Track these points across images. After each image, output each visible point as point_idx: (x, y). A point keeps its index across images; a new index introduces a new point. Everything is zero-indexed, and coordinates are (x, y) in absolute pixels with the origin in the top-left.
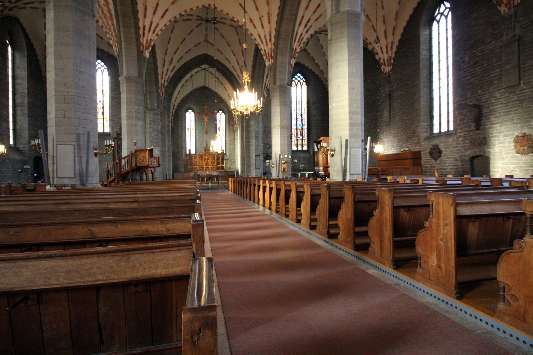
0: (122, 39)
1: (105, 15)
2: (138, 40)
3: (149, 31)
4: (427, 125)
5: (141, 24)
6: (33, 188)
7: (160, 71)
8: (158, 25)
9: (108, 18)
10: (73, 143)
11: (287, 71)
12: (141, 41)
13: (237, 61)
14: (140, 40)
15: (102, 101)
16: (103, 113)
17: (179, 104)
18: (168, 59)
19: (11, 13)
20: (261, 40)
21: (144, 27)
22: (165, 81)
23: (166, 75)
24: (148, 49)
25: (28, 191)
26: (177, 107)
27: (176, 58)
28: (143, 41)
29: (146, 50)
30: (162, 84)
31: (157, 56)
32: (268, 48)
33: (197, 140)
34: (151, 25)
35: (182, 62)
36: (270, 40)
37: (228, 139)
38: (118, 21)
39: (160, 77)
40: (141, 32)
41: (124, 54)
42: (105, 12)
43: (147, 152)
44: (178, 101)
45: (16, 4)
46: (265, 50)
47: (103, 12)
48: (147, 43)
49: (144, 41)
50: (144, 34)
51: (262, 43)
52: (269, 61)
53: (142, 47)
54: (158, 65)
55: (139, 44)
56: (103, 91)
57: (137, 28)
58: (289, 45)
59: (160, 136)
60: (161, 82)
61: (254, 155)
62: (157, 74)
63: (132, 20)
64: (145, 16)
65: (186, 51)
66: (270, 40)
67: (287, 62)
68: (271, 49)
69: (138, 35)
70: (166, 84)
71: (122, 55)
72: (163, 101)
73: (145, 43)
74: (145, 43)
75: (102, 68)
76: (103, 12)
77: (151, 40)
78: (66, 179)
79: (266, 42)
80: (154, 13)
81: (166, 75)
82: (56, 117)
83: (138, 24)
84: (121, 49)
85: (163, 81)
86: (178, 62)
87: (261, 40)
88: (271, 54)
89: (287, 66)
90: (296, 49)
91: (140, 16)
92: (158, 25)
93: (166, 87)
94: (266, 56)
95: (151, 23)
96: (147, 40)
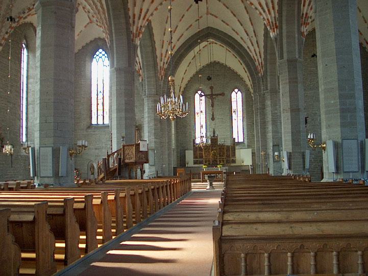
0: (113, 31)
1: (98, 10)
2: (128, 29)
3: (139, 19)
5: (131, 13)
6: (26, 185)
7: (158, 53)
8: (148, 10)
9: (101, 13)
10: (51, 145)
11: (297, 41)
12: (131, 30)
13: (246, 32)
14: (130, 29)
15: (102, 92)
16: (103, 104)
17: (186, 85)
18: (167, 38)
19: (26, 20)
20: (263, 8)
21: (134, 15)
22: (164, 63)
23: (165, 57)
24: (139, 36)
25: (22, 188)
26: (185, 89)
27: (175, 36)
28: (133, 29)
29: (136, 37)
30: (161, 67)
31: (155, 37)
32: (271, 17)
33: (208, 125)
34: (141, 12)
35: (182, 40)
36: (273, 8)
37: (245, 123)
38: (109, 15)
39: (158, 60)
40: (131, 21)
41: (115, 46)
42: (99, 8)
43: (134, 148)
44: (185, 82)
45: (29, 13)
46: (268, 19)
47: (97, 8)
48: (137, 31)
49: (134, 29)
50: (134, 22)
51: (264, 11)
52: (274, 31)
53: (132, 35)
54: (156, 47)
55: (129, 32)
56: (103, 80)
57: (127, 17)
58: (296, 11)
59: (159, 125)
60: (160, 64)
61: (271, 144)
62: (155, 57)
63: (122, 11)
65: (186, 28)
66: (273, 8)
67: (296, 30)
68: (275, 17)
69: (127, 23)
70: (166, 66)
71: (113, 47)
72: (162, 86)
73: (135, 32)
74: (135, 32)
75: (103, 57)
76: (97, 8)
77: (141, 26)
78: (46, 179)
79: (269, 10)
81: (165, 57)
82: (40, 123)
83: (128, 14)
84: (113, 40)
85: (162, 63)
86: (178, 40)
87: (263, 8)
88: (276, 24)
89: (296, 35)
90: (307, 14)
92: (148, 10)
93: (165, 70)
94: (270, 25)
95: (141, 10)
96: (137, 27)
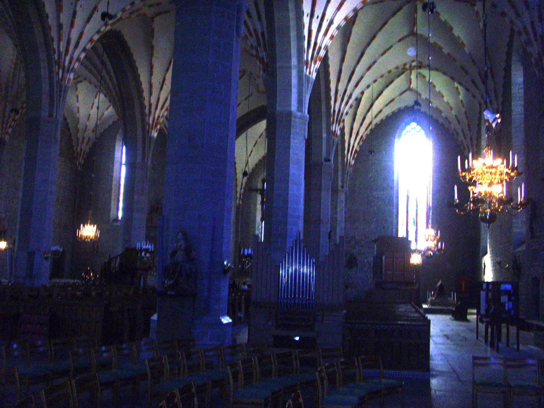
2: (143, 120)
3: (156, 108)
4: (522, 222)
5: (146, 103)
21: (150, 105)
40: (147, 111)
57: (142, 106)
64: (151, 93)
73: (151, 122)
74: (151, 122)
80: (161, 89)
91: (146, 94)
96: (154, 118)
